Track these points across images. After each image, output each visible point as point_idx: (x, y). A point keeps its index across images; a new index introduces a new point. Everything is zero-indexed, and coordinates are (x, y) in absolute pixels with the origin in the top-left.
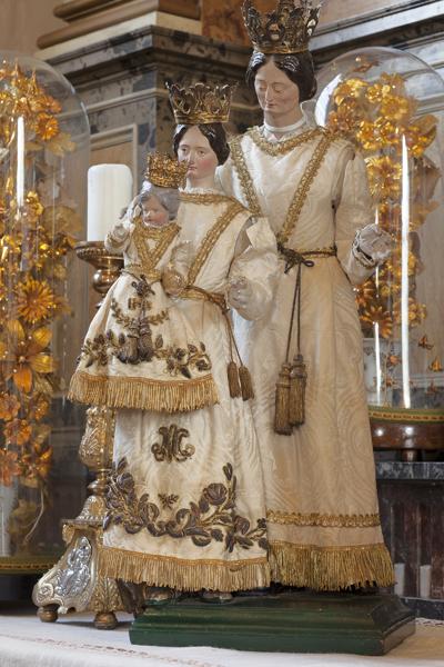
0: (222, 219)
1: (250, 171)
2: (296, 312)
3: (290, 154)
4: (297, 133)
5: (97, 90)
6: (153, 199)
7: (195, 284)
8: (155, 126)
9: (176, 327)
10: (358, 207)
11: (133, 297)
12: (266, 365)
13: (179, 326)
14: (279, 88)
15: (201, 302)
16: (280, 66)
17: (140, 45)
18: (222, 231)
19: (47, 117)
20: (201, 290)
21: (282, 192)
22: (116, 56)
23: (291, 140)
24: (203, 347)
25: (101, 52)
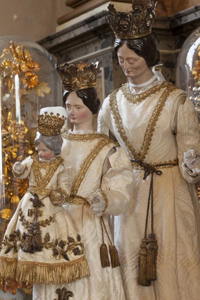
0: (94, 150)
1: (120, 113)
2: (150, 205)
3: (144, 102)
4: (149, 88)
5: (85, 48)
6: (41, 143)
7: (78, 194)
8: (112, 69)
9: (61, 226)
10: (188, 134)
11: (31, 208)
12: (132, 240)
13: (59, 228)
14: (131, 61)
15: (81, 206)
16: (130, 47)
17: (100, 22)
18: (93, 159)
19: (31, 74)
20: (81, 198)
21: (138, 128)
22: (89, 29)
23: (145, 92)
24: (79, 238)
25: (82, 27)
